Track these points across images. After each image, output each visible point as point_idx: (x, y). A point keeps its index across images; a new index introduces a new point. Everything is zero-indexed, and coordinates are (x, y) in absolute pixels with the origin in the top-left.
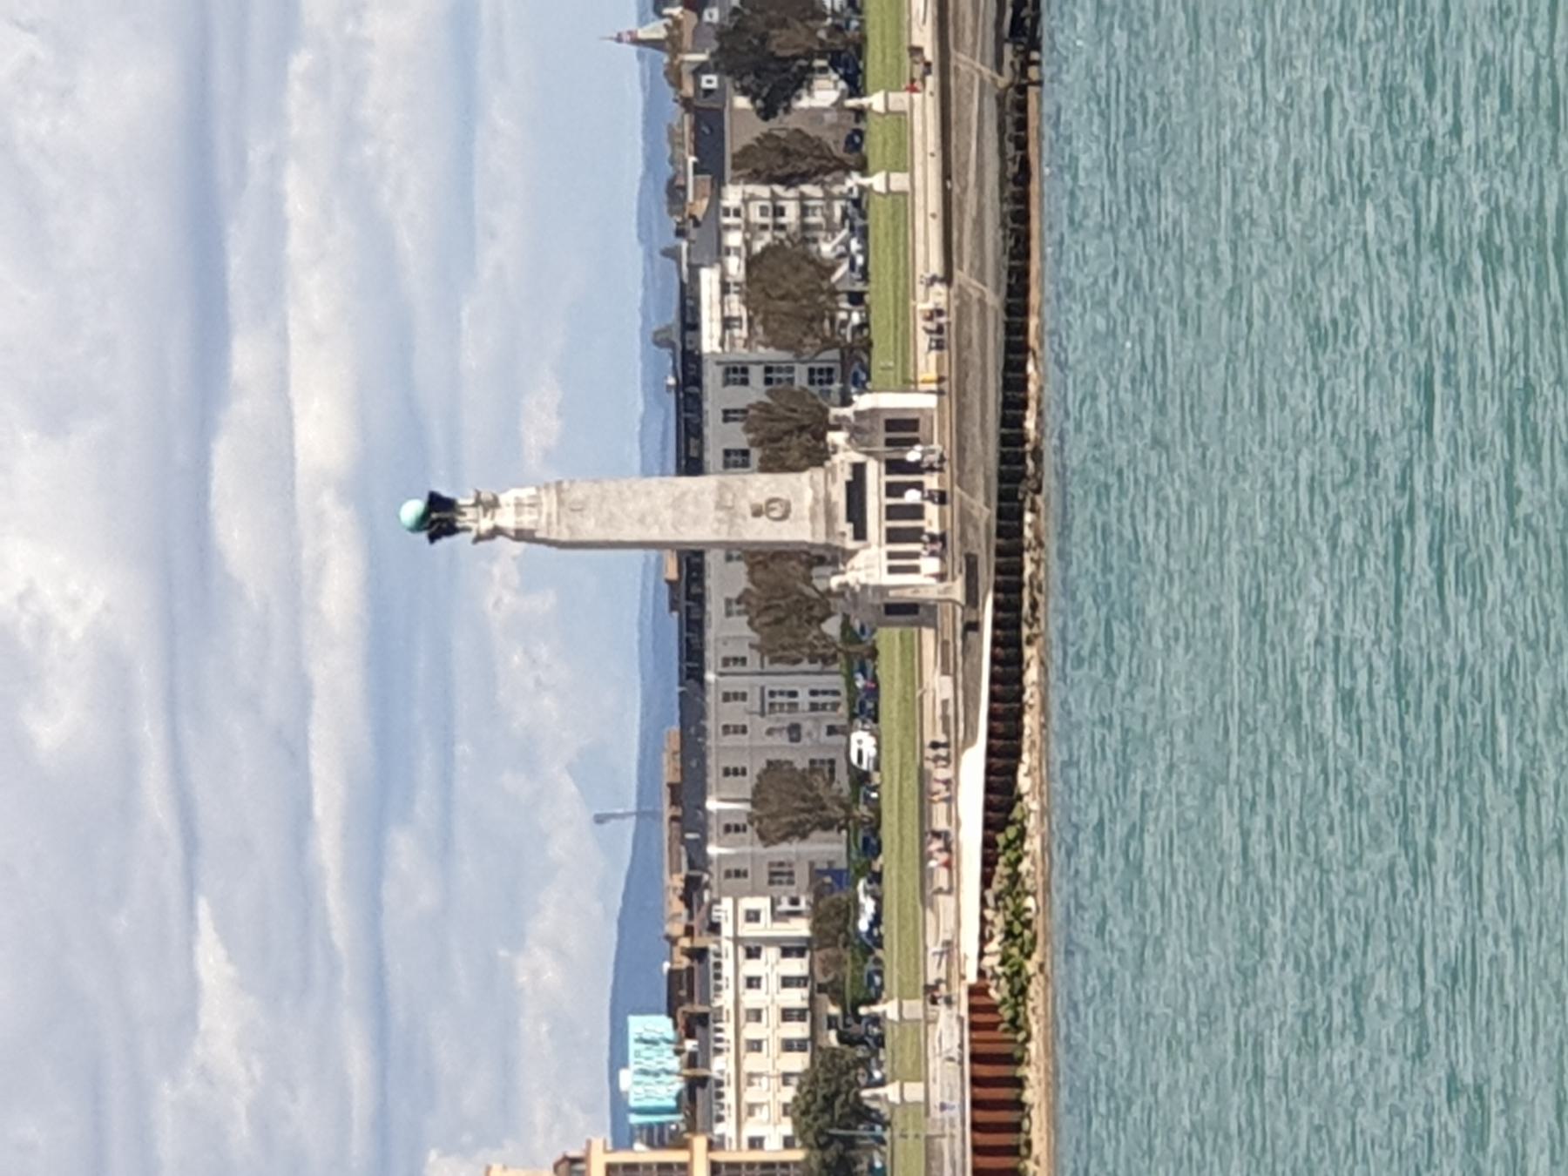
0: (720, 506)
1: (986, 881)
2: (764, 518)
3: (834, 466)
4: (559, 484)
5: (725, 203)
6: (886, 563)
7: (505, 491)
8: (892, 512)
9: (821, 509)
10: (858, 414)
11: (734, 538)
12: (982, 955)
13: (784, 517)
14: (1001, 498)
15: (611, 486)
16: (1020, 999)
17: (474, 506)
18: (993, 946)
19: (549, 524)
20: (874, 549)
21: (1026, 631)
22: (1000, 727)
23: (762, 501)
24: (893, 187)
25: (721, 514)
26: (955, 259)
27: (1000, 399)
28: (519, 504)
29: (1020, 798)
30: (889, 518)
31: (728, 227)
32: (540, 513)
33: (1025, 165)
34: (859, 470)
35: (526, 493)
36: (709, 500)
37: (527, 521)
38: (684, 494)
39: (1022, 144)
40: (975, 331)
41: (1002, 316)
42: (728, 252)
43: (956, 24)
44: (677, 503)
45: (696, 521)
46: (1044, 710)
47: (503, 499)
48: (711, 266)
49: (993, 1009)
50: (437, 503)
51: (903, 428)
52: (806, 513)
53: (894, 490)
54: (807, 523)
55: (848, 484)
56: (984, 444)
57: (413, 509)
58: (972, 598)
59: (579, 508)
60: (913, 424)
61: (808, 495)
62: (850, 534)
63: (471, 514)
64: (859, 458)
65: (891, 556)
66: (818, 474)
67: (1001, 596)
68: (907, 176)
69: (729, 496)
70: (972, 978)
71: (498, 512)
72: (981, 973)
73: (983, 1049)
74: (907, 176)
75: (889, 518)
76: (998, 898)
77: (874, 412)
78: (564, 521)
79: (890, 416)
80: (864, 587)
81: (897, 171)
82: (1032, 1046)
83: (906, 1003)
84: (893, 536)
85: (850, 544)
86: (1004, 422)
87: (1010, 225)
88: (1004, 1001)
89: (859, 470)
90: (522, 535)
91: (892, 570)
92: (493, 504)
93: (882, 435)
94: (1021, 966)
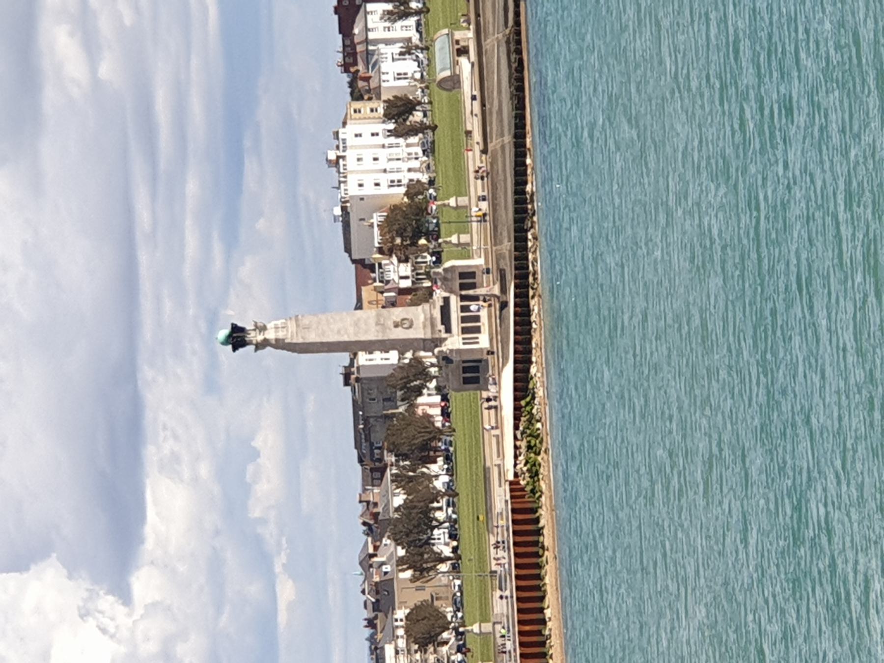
0: (377, 324)
1: (516, 427)
2: (400, 329)
3: (434, 301)
4: (297, 316)
5: (395, 617)
6: (461, 341)
7: (270, 322)
8: (464, 320)
9: (428, 323)
10: (445, 270)
11: (386, 338)
12: (515, 465)
13: (410, 327)
14: (516, 240)
15: (323, 317)
16: (536, 479)
17: (255, 330)
18: (521, 458)
19: (292, 336)
20: (456, 337)
21: (531, 293)
22: (520, 347)
23: (399, 320)
24: (483, 630)
25: (378, 328)
26: (489, 140)
27: (513, 172)
28: (276, 328)
29: (532, 378)
30: (462, 322)
31: (397, 627)
32: (287, 331)
33: (521, 62)
34: (446, 300)
35: (279, 323)
36: (372, 322)
37: (281, 335)
38: (359, 320)
39: (519, 52)
41: (513, 150)
42: (398, 637)
43: (484, 30)
44: (356, 324)
45: (366, 332)
46: (533, 135)
47: (268, 326)
48: (390, 643)
49: (523, 489)
50: (235, 329)
51: (468, 279)
52: (421, 325)
53: (464, 309)
54: (422, 330)
55: (441, 307)
56: (507, 214)
57: (223, 333)
58: (504, 290)
59: (307, 328)
60: (472, 275)
61: (422, 318)
62: (443, 331)
63: (253, 334)
64: (446, 294)
65: (464, 339)
66: (426, 306)
67: (517, 281)
68: (469, 235)
69: (382, 320)
70: (511, 477)
71: (266, 332)
72: (516, 475)
73: (517, 506)
74: (469, 235)
75: (462, 322)
76: (523, 433)
77: (453, 268)
78: (299, 335)
79: (461, 270)
80: (451, 351)
81: (464, 233)
82: (543, 499)
83: (483, 625)
84: (465, 331)
85: (444, 335)
86: (516, 192)
87: (515, 92)
88: (528, 484)
89: (446, 300)
90: (280, 344)
91: (464, 344)
92: (263, 329)
93: (457, 282)
94: (536, 460)
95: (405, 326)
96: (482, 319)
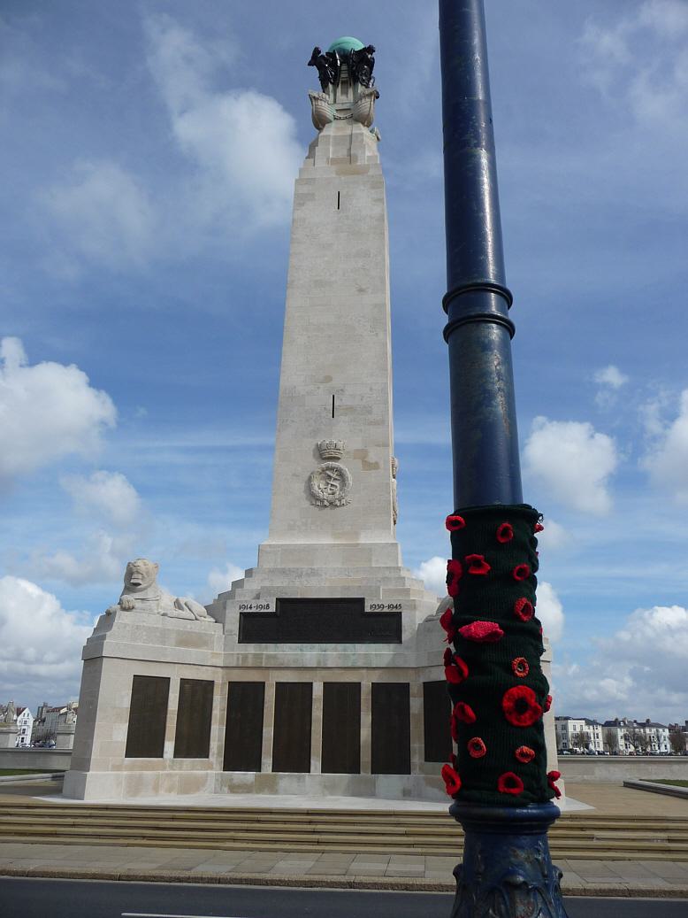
34: (385, 626)
40: (595, 843)
91: (148, 692)
95: (319, 485)
96: (287, 779)
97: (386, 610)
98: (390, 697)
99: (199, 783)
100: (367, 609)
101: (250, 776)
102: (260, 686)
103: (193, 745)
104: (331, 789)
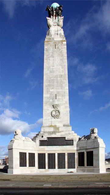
34: (70, 143)
62: (42, 139)
84: (42, 156)
89: (70, 143)
91: (22, 155)
97: (70, 139)
98: (71, 155)
99: (35, 171)
100: (66, 139)
101: (44, 170)
102: (49, 168)
103: (32, 164)
104: (88, 171)
